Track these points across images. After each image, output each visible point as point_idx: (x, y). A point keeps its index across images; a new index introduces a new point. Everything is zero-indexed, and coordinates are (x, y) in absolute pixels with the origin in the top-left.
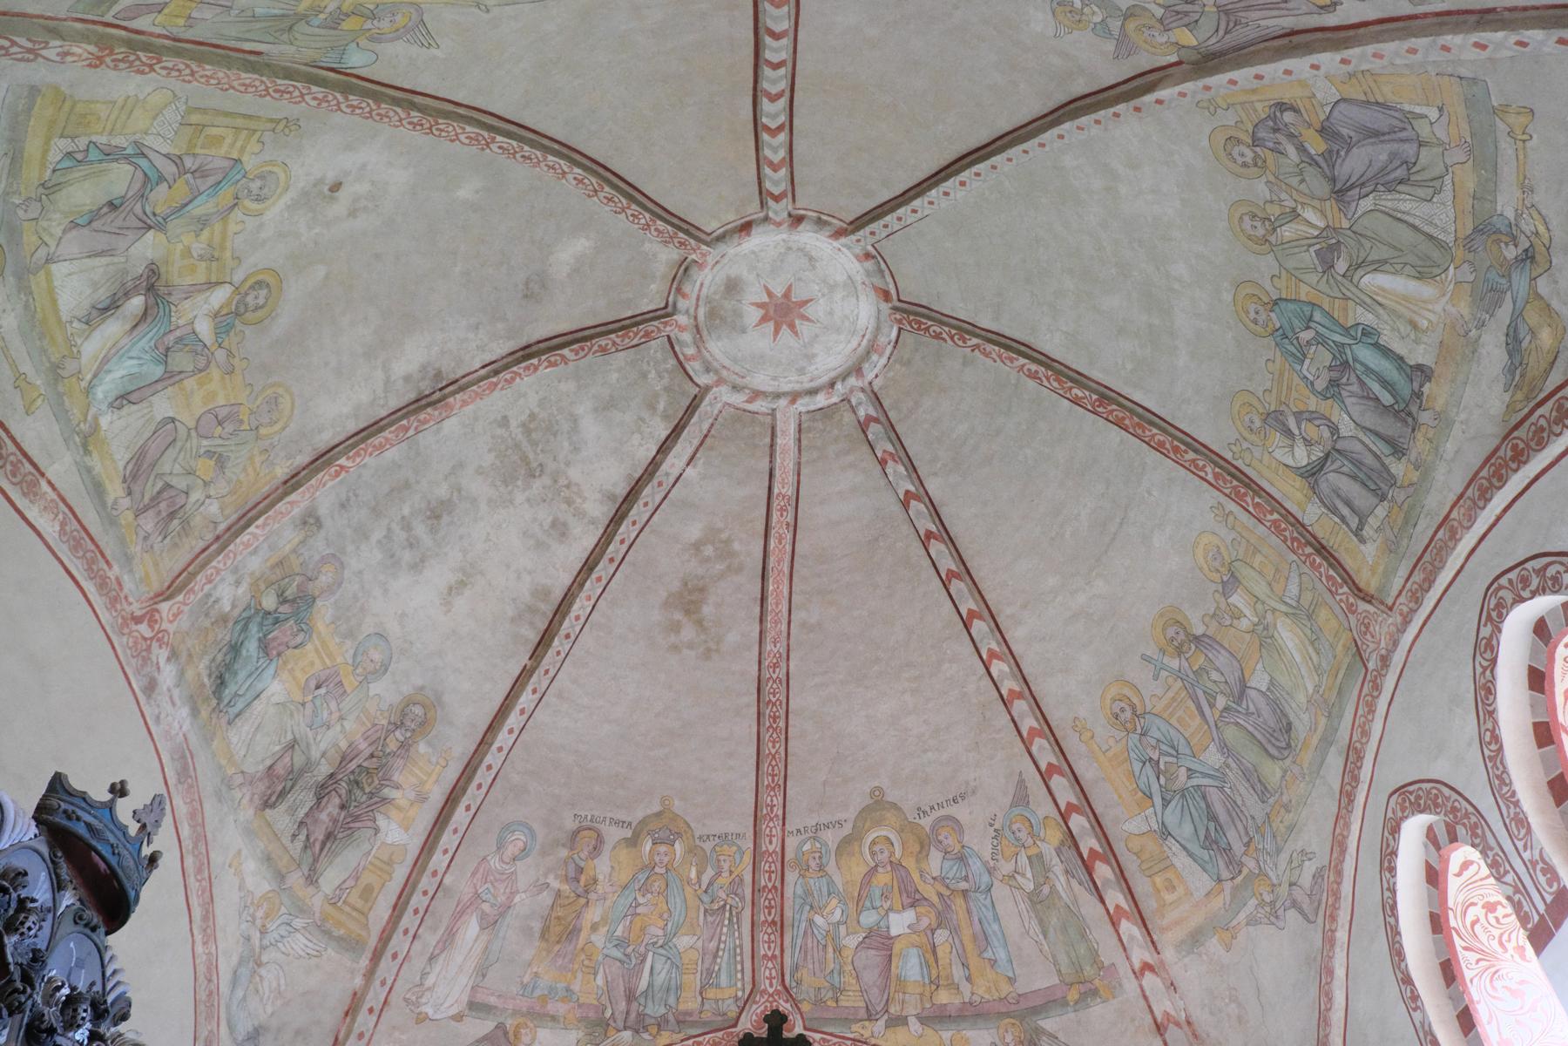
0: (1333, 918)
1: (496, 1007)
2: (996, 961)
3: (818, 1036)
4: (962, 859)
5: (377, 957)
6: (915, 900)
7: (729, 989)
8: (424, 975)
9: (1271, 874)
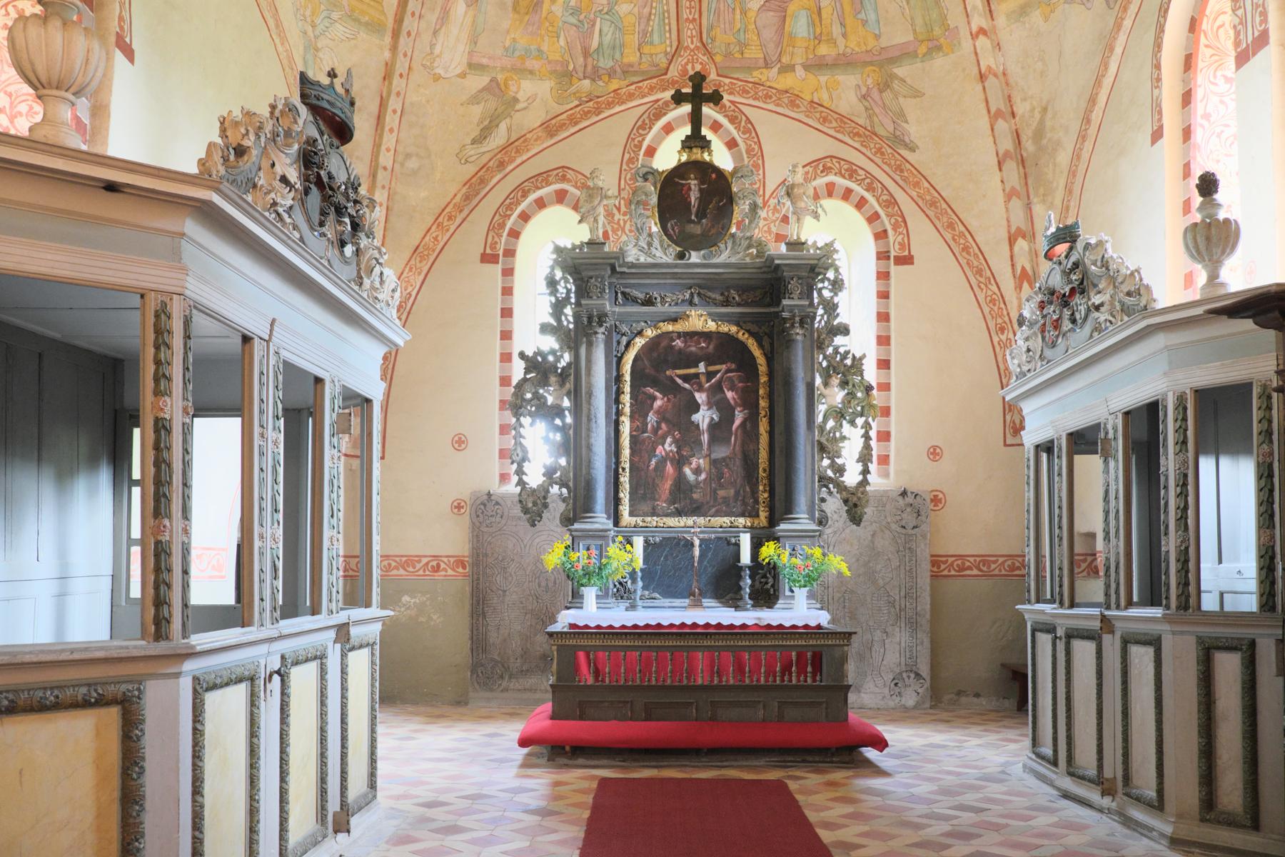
0: (1125, 9)
1: (488, 66)
2: (867, 21)
3: (727, 81)
5: (396, 35)
7: (660, 46)
8: (432, 46)
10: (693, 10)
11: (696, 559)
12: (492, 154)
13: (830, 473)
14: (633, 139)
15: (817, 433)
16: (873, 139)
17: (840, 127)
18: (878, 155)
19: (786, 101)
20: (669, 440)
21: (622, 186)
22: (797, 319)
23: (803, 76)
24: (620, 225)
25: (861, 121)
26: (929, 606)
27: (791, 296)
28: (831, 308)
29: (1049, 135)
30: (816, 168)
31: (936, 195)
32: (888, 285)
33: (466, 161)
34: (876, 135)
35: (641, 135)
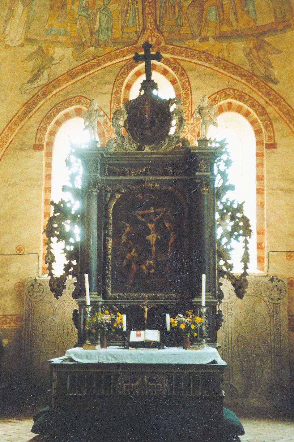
1: (36, 40)
3: (171, 47)
10: (151, 8)
11: (146, 319)
12: (39, 88)
13: (224, 269)
14: (119, 80)
15: (216, 246)
17: (235, 71)
18: (256, 87)
19: (203, 57)
20: (133, 250)
21: (112, 107)
24: (111, 129)
28: (224, 175)
30: (221, 94)
31: (290, 108)
33: (25, 93)
35: (123, 77)
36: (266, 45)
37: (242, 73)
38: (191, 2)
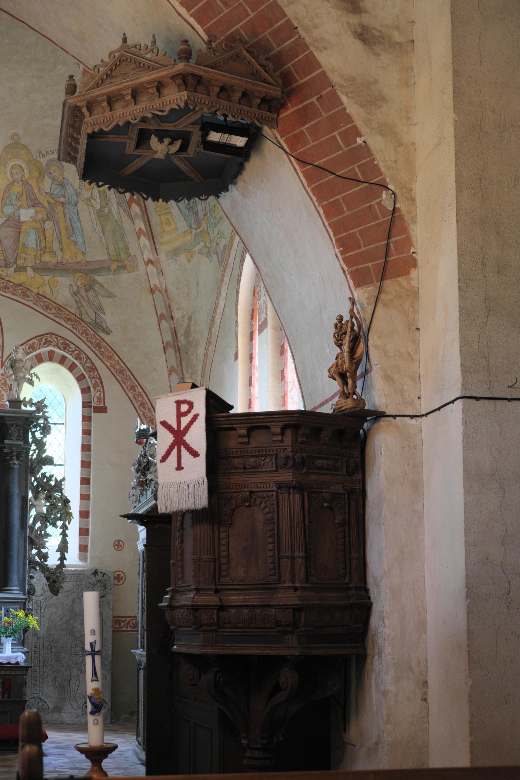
2: (77, 242)
4: (62, 185)
6: (34, 203)
9: (211, 235)
15: (28, 531)
16: (81, 324)
18: (84, 335)
19: (19, 291)
22: (15, 454)
23: (33, 275)
25: (73, 310)
26: (110, 652)
27: (11, 438)
28: (41, 445)
29: (193, 335)
31: (123, 366)
32: (90, 426)
34: (83, 321)
36: (97, 286)
37: (68, 317)
38: (5, 221)
